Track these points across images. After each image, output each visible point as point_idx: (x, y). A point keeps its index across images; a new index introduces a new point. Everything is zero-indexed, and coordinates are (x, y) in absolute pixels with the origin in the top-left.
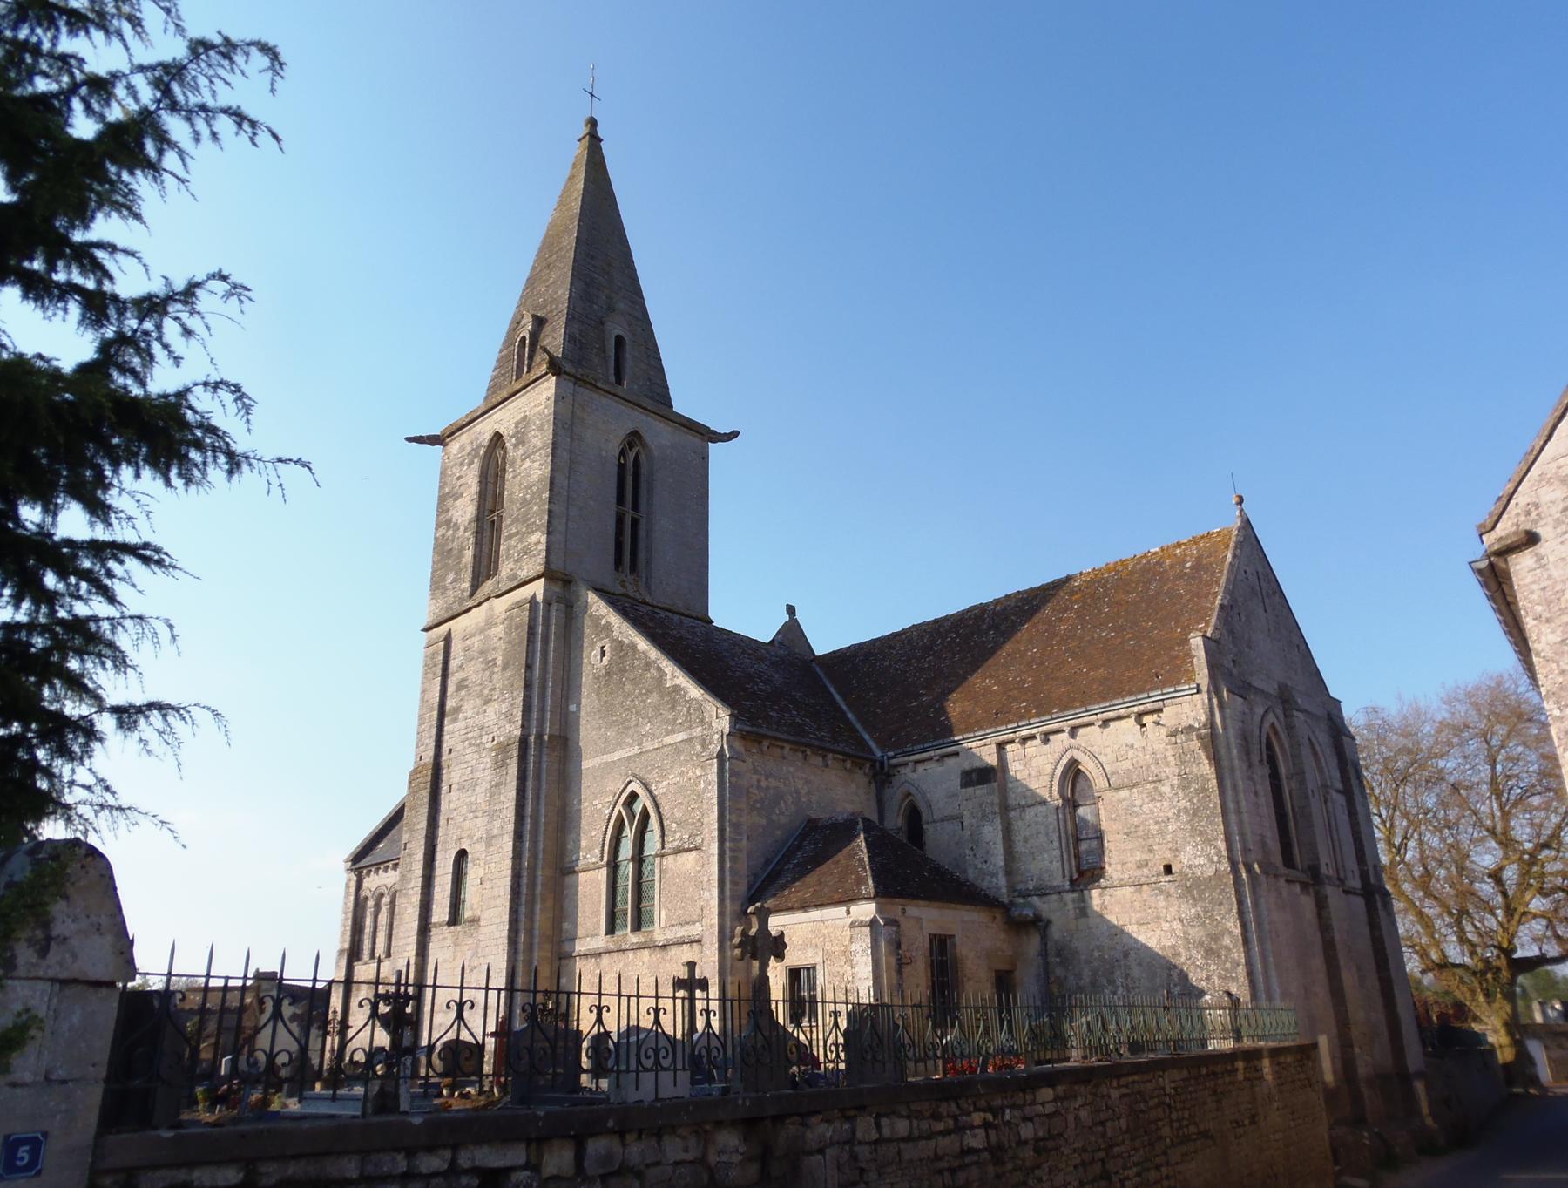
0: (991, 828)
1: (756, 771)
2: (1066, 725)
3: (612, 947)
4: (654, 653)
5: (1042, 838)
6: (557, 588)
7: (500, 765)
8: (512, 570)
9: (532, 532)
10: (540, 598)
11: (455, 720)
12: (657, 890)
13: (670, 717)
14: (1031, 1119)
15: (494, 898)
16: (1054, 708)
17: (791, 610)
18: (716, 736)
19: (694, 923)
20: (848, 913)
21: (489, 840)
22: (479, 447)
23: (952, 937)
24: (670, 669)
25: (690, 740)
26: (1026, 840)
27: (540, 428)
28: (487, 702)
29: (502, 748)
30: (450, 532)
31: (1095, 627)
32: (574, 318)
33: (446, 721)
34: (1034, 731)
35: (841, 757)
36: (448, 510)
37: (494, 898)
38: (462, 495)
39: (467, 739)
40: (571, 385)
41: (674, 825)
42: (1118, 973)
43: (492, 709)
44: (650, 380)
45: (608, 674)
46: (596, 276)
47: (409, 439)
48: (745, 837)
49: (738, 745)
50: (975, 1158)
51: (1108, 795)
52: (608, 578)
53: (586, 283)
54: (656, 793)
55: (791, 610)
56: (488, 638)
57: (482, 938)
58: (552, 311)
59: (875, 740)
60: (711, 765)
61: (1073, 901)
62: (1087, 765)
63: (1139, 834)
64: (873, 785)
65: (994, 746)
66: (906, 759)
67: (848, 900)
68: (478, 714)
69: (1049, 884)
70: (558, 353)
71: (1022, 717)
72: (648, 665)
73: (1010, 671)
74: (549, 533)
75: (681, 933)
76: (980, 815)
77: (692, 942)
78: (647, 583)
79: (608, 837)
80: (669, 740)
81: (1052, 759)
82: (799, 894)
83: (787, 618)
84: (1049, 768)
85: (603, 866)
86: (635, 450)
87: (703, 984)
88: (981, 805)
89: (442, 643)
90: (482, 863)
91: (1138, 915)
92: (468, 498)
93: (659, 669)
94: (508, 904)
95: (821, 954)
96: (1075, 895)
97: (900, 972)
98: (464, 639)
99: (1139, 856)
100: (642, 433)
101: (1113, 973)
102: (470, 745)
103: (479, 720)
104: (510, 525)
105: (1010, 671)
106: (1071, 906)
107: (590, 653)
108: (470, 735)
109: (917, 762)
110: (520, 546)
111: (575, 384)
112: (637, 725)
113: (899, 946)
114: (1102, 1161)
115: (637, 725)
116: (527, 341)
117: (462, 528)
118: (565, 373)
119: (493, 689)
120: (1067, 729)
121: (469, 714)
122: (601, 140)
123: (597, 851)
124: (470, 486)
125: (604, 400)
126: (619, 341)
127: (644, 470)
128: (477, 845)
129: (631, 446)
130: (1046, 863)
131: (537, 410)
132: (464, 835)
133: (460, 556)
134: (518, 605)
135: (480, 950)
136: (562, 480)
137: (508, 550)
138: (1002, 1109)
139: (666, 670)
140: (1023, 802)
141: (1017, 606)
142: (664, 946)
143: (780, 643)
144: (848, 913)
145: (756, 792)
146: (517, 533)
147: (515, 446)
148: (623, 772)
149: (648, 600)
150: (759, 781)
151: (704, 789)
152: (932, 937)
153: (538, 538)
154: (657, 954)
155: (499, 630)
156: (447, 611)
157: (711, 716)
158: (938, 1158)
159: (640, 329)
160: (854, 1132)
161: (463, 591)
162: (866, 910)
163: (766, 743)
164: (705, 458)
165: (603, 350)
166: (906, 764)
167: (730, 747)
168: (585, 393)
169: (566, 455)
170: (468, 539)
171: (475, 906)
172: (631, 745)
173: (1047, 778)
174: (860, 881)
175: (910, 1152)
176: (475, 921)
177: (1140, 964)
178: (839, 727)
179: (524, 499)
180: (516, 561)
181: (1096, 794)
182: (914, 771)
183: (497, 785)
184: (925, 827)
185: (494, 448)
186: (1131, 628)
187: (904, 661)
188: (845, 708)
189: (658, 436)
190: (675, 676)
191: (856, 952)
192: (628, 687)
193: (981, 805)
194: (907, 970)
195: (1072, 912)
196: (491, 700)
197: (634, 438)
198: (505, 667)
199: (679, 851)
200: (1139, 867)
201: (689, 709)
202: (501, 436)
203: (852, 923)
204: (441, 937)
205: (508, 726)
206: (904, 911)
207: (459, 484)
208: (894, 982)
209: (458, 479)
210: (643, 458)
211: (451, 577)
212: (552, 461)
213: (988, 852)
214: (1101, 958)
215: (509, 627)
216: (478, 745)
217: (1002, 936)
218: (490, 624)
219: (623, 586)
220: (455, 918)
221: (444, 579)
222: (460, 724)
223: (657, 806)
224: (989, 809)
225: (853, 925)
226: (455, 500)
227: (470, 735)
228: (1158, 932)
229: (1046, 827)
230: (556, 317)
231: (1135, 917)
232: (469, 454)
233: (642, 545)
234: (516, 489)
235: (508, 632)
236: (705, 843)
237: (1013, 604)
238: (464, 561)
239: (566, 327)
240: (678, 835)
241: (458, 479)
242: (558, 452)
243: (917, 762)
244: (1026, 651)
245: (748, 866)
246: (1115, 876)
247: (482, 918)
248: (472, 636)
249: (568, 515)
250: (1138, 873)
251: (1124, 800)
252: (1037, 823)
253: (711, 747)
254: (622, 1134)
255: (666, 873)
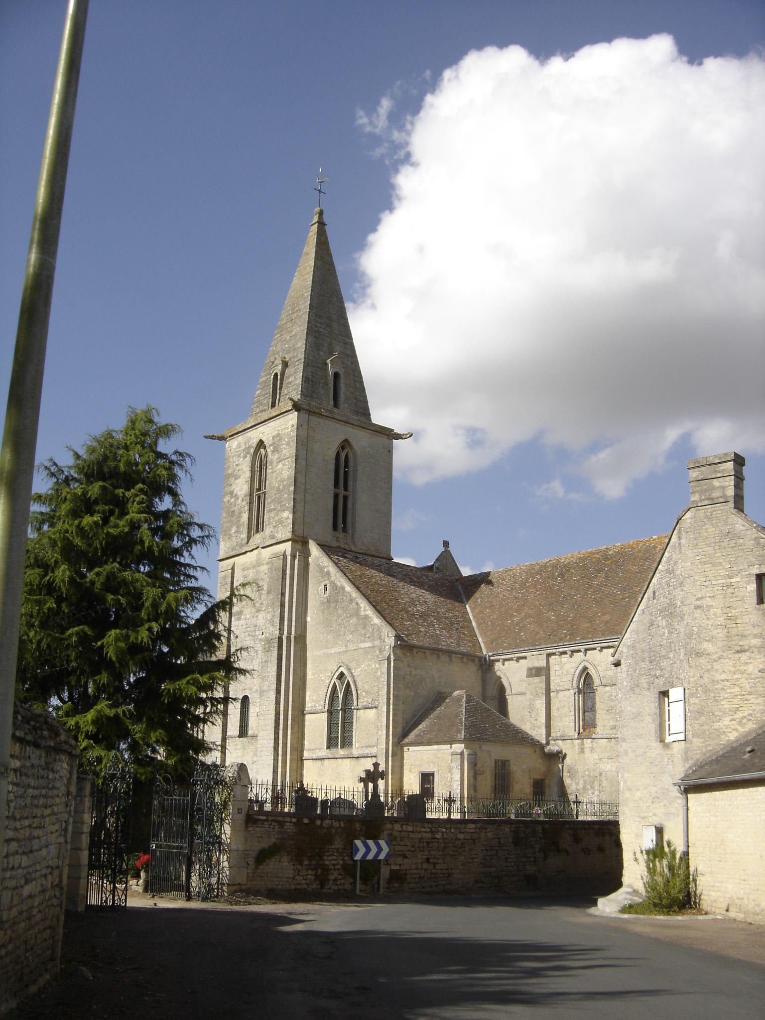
0: (540, 702)
1: (409, 666)
2: (582, 648)
3: (330, 756)
4: (355, 594)
5: (566, 709)
6: (299, 546)
7: (267, 650)
8: (272, 532)
9: (284, 510)
10: (288, 553)
11: (239, 619)
12: (354, 727)
13: (363, 632)
14: (463, 833)
15: (266, 725)
16: (578, 637)
17: (446, 544)
18: (387, 647)
19: (373, 746)
20: (451, 747)
21: (262, 693)
22: (250, 447)
23: (508, 761)
24: (363, 604)
25: (374, 647)
26: (558, 709)
27: (288, 444)
28: (258, 611)
29: (269, 641)
30: (233, 500)
31: (612, 586)
32: (308, 364)
33: (233, 619)
34: (566, 649)
35: (461, 656)
36: (231, 485)
37: (266, 725)
38: (240, 477)
39: (247, 631)
40: (306, 416)
41: (364, 693)
42: (596, 783)
43: (261, 615)
44: (356, 398)
45: (328, 601)
46: (322, 330)
47: (206, 437)
48: (402, 702)
49: (399, 652)
50: (437, 840)
51: (600, 689)
52: (328, 536)
53: (315, 337)
54: (354, 674)
55: (446, 544)
56: (258, 572)
57: (259, 746)
58: (294, 357)
59: (484, 642)
60: (384, 663)
61: (578, 744)
62: (592, 671)
63: (613, 711)
64: (480, 671)
65: (545, 655)
66: (499, 657)
67: (451, 742)
68: (253, 617)
69: (568, 734)
70: (297, 397)
71: (561, 640)
72: (351, 600)
73: (563, 607)
74: (294, 513)
75: (367, 751)
76: (535, 694)
77: (372, 757)
78: (352, 536)
79: (328, 695)
80: (362, 645)
81: (574, 665)
82: (428, 735)
83: (443, 549)
84: (572, 671)
85: (325, 712)
86: (346, 451)
87: (383, 775)
88: (536, 688)
89: (230, 571)
90: (258, 705)
91: (609, 754)
92: (243, 480)
93: (357, 604)
94: (273, 729)
95: (437, 766)
96: (579, 741)
97: (475, 778)
98: (244, 570)
99: (612, 723)
100: (349, 440)
101: (593, 783)
102: (249, 635)
103: (254, 621)
104: (270, 503)
105: (563, 607)
106: (577, 747)
107: (318, 588)
108: (248, 629)
109: (505, 660)
110: (277, 518)
111: (309, 415)
112: (344, 634)
113: (475, 765)
114: (497, 851)
115: (344, 634)
116: (279, 377)
117: (240, 499)
118: (303, 409)
119: (262, 604)
120: (583, 650)
121: (248, 616)
122: (325, 225)
123: (322, 703)
124: (245, 472)
125: (327, 422)
126: (336, 375)
127: (351, 464)
128: (254, 694)
129: (343, 448)
130: (568, 723)
131: (286, 431)
132: (246, 687)
133: (240, 517)
134: (276, 556)
135: (258, 753)
136: (301, 479)
137: (270, 519)
138: (451, 828)
139: (361, 606)
140: (558, 688)
141: (576, 563)
142: (358, 757)
143: (437, 568)
144: (451, 747)
145: (409, 677)
146: (275, 509)
147: (273, 452)
148: (337, 660)
149: (353, 548)
150: (410, 672)
151: (380, 676)
152: (496, 761)
153: (288, 515)
154: (354, 761)
155: (265, 568)
156: (232, 550)
157: (385, 635)
158: (422, 838)
159: (349, 363)
160: (393, 827)
161: (242, 539)
162: (459, 747)
163: (415, 650)
164: (390, 451)
165: (326, 384)
166: (498, 661)
167: (395, 654)
168: (314, 419)
169: (304, 462)
170: (244, 507)
171: (254, 728)
172: (341, 646)
173: (571, 676)
174: (459, 732)
175: (412, 835)
176: (255, 737)
177: (607, 779)
178: (464, 634)
179: (278, 488)
180: (275, 527)
181: (595, 688)
182: (504, 665)
183: (266, 662)
184: (507, 697)
185: (259, 449)
186: (629, 590)
187: (509, 590)
188: (471, 617)
189: (360, 440)
190: (366, 609)
191: (453, 767)
192: (340, 611)
193: (536, 688)
194: (479, 778)
195: (577, 750)
196: (260, 610)
197: (345, 444)
198: (269, 592)
199: (366, 708)
200: (611, 729)
201: (373, 629)
202: (263, 442)
203: (452, 753)
204: (235, 743)
205: (271, 628)
206: (480, 747)
207: (237, 469)
208: (472, 783)
209: (237, 465)
210: (350, 455)
211: (234, 529)
212: (295, 467)
213: (537, 715)
214: (589, 775)
215: (271, 569)
216: (254, 636)
217: (540, 761)
218: (258, 564)
219: (338, 541)
220: (243, 732)
221: (230, 530)
222: (242, 622)
223: (355, 682)
224: (540, 691)
225: (452, 754)
226: (236, 479)
227: (248, 629)
228: (617, 763)
229: (569, 703)
230: (297, 363)
231: (607, 755)
232: (243, 451)
233: (349, 513)
234: (274, 481)
235: (271, 570)
236: (380, 705)
237: (574, 560)
238: (242, 520)
239: (303, 372)
240: (366, 699)
241: (237, 465)
242: (299, 461)
243: (505, 660)
244: (574, 595)
245: (403, 718)
246: (600, 732)
247: (259, 735)
248: (248, 569)
249: (305, 501)
250: (611, 732)
251: (608, 692)
252: (564, 701)
253: (384, 653)
254: (331, 820)
255: (359, 719)
